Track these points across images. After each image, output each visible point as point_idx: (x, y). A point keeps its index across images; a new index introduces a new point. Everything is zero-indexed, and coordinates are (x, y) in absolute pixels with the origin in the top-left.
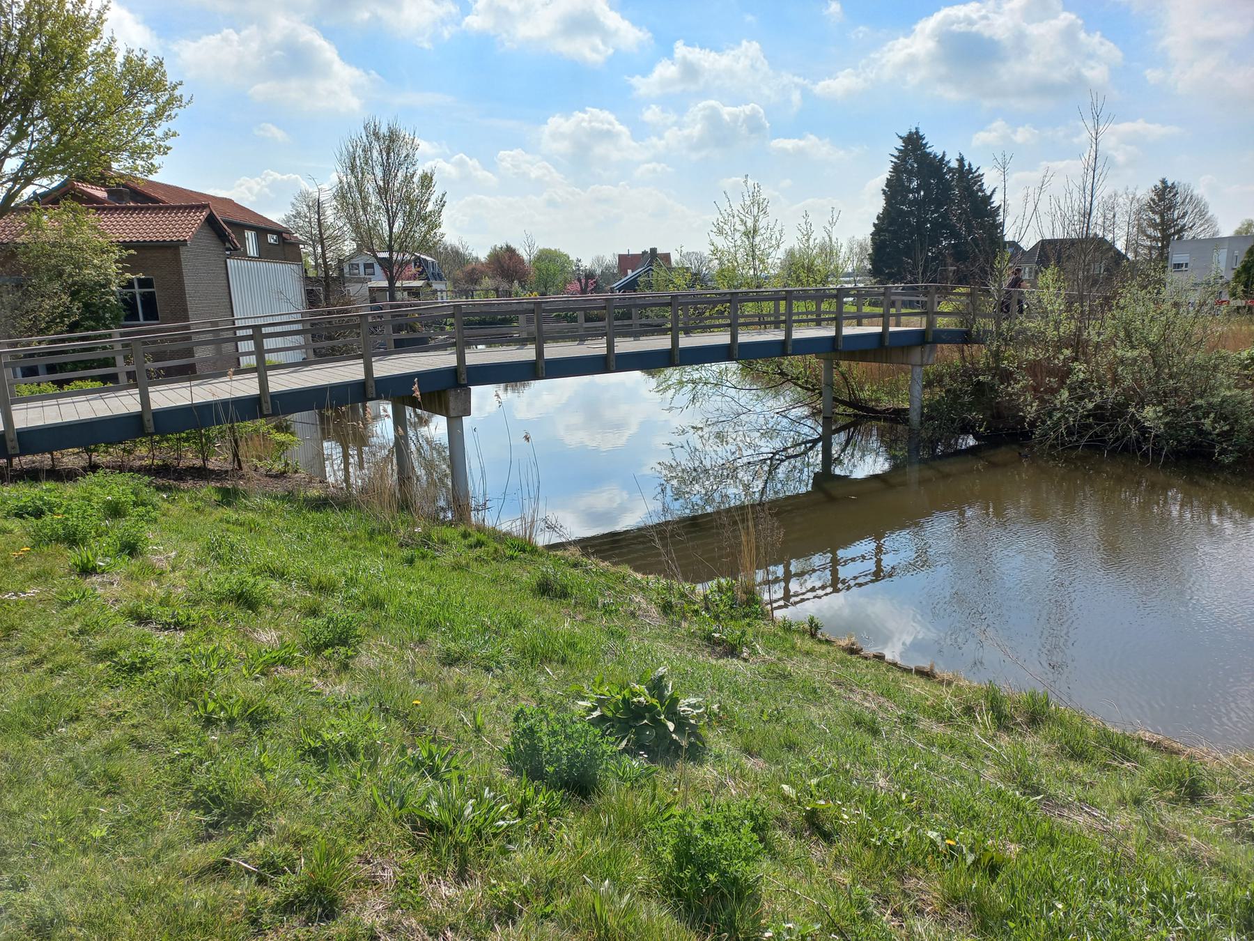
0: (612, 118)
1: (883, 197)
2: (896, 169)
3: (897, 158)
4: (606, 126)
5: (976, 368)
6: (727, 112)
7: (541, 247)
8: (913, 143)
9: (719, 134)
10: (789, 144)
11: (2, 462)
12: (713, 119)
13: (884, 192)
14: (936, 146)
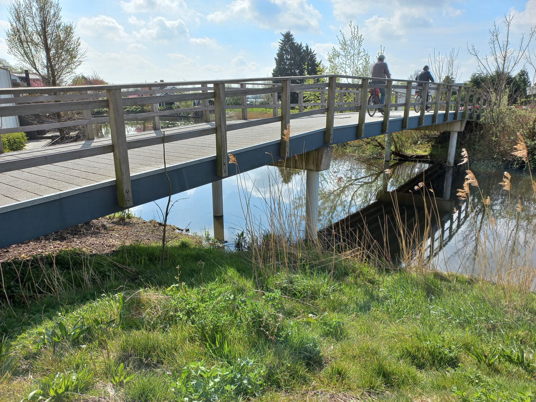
0: (114, 21)
1: (275, 62)
2: (282, 49)
3: (281, 44)
4: (111, 24)
5: (441, 157)
6: (168, 23)
7: (89, 74)
8: (288, 37)
9: (166, 33)
10: (198, 41)
11: (82, 401)
12: (162, 25)
13: (276, 59)
14: (298, 39)
